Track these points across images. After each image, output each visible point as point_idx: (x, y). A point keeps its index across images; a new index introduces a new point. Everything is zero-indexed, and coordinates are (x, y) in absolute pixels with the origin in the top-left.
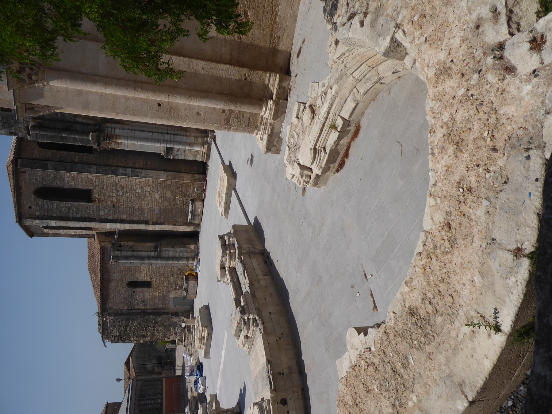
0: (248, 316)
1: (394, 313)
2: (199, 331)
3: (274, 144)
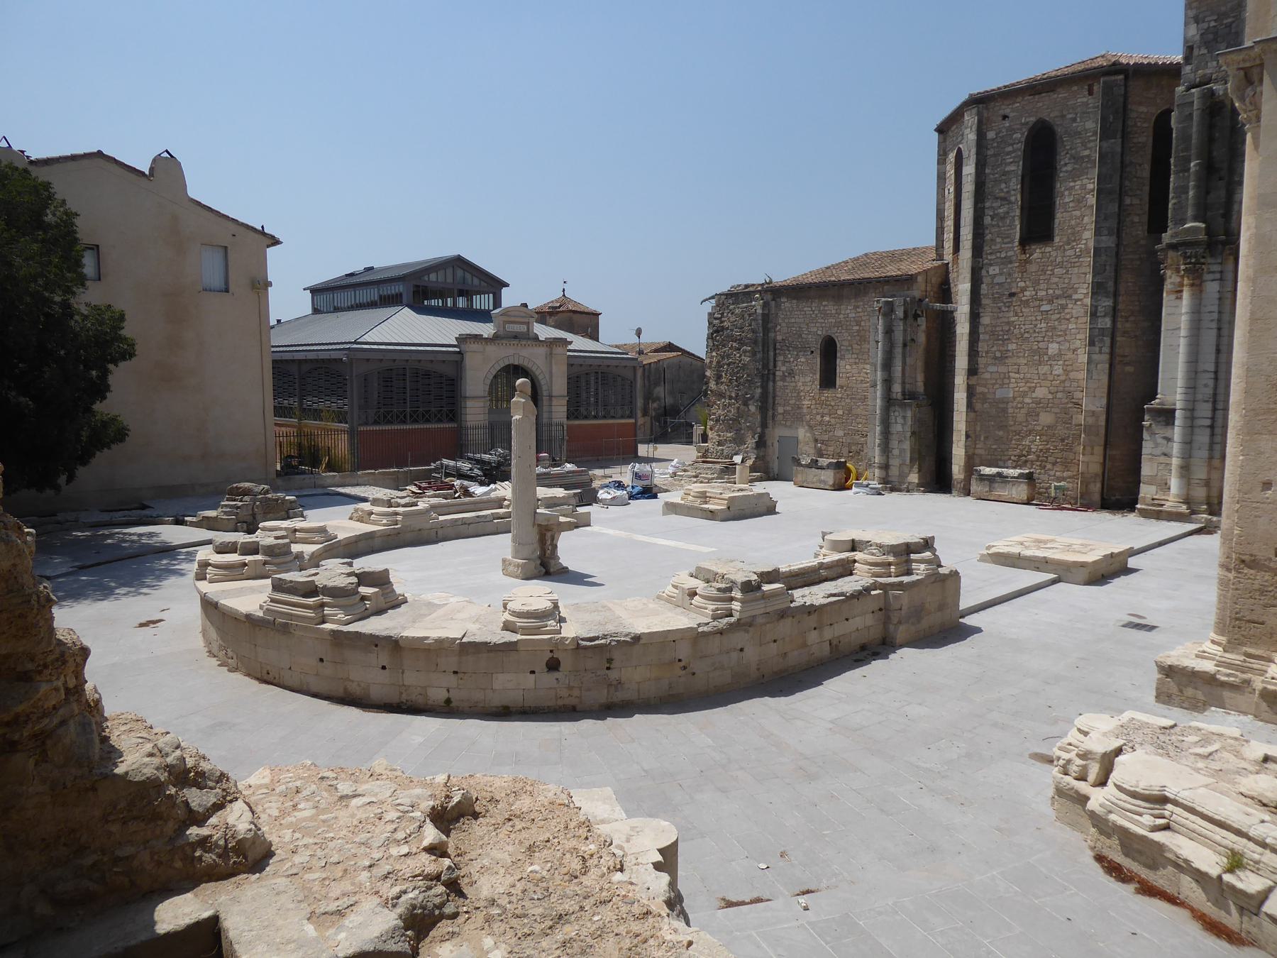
0: (736, 600)
1: (690, 944)
2: (721, 492)
3: (1183, 687)
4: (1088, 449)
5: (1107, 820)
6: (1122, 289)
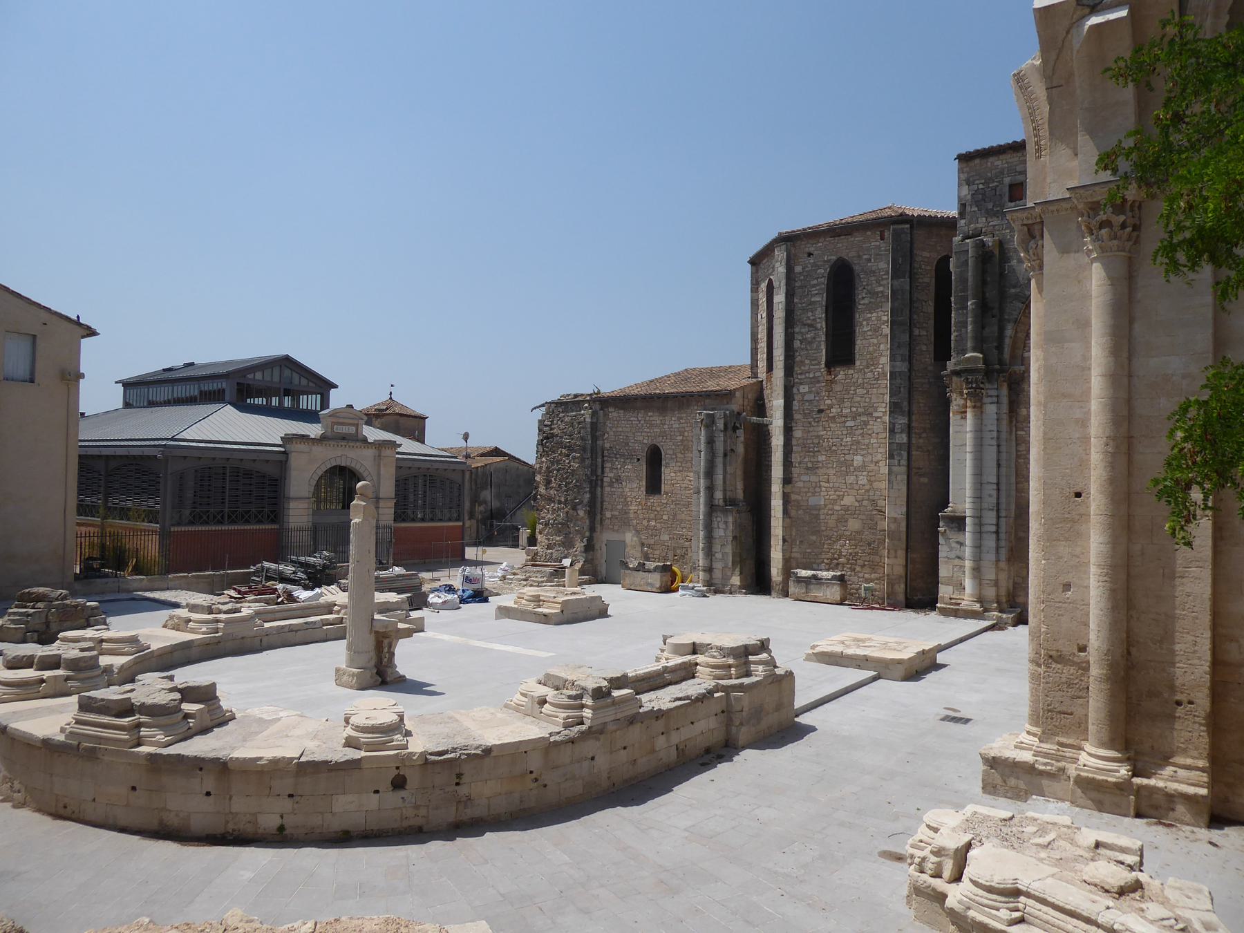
2: (554, 596)
3: (1005, 777)
4: (892, 552)
5: (966, 917)
6: (915, 408)
